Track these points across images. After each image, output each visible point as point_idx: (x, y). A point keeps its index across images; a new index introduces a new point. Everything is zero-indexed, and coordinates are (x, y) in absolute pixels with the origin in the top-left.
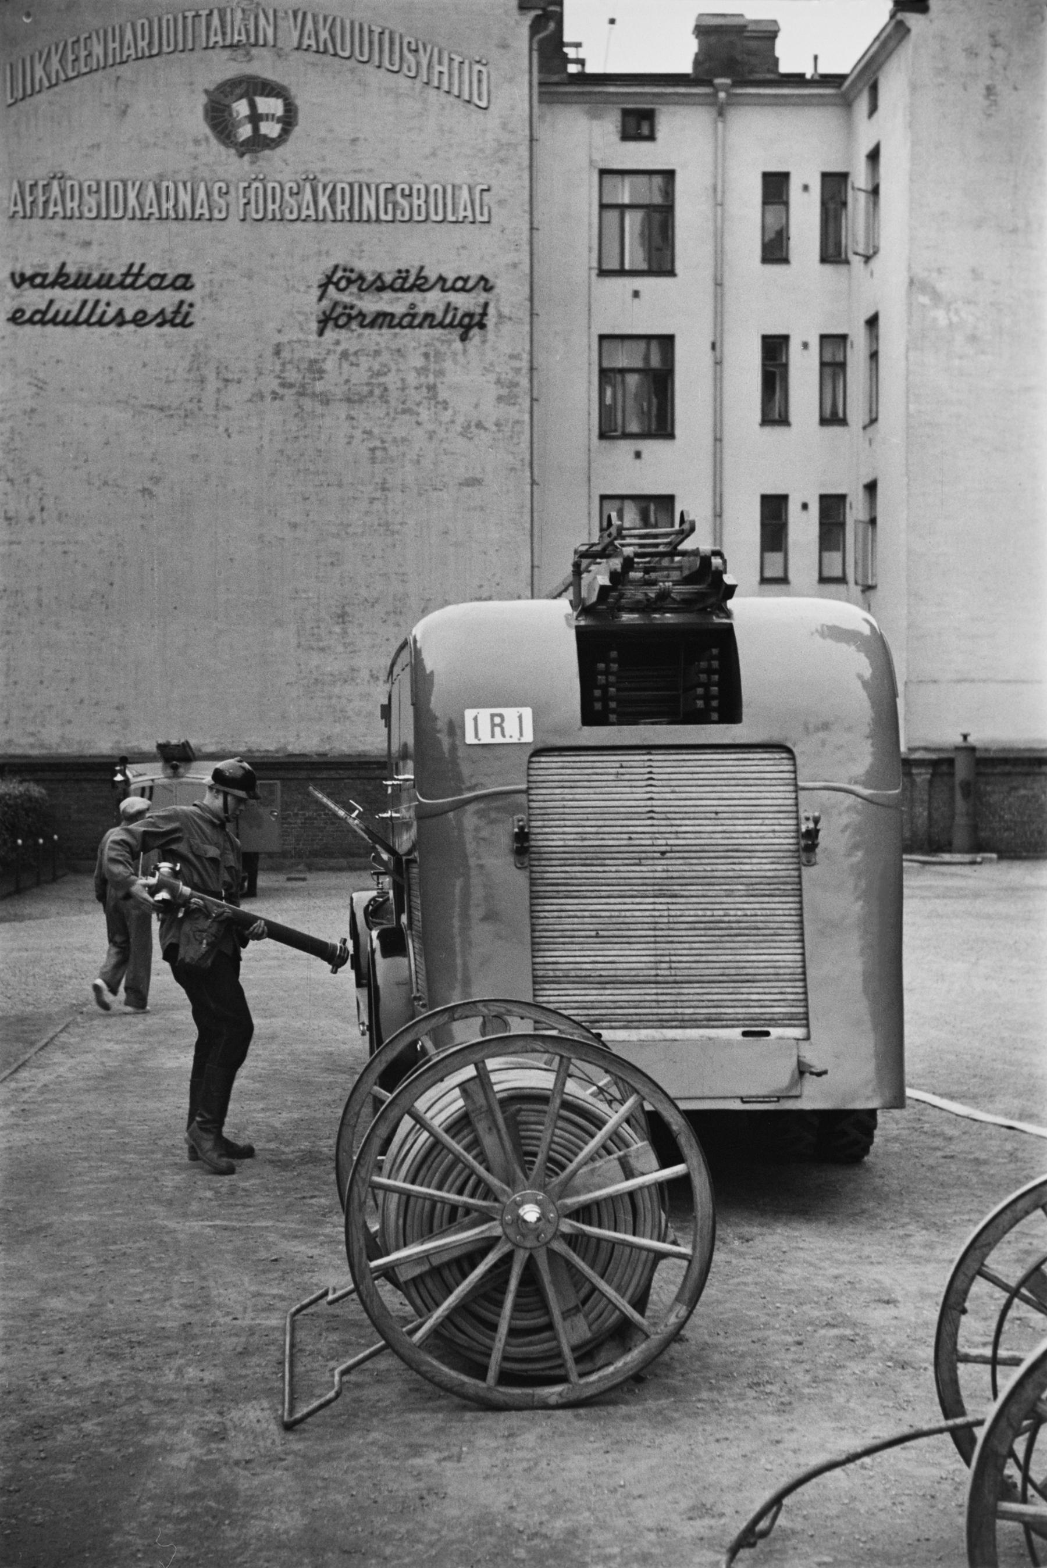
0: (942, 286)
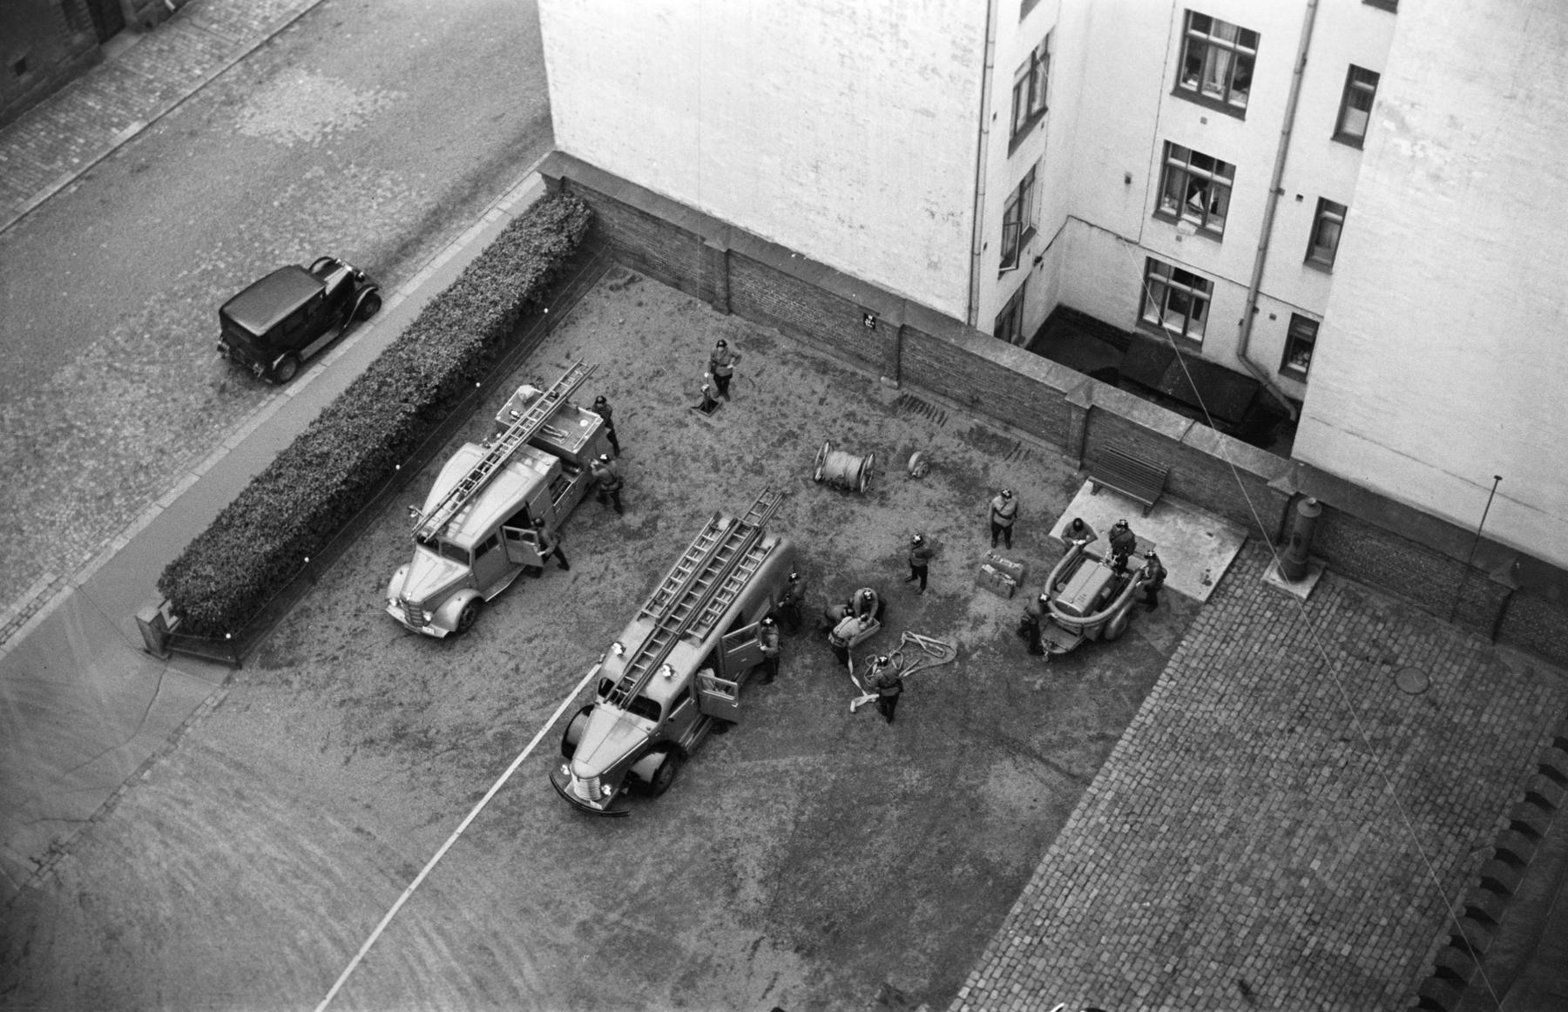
0: (1412, 119)
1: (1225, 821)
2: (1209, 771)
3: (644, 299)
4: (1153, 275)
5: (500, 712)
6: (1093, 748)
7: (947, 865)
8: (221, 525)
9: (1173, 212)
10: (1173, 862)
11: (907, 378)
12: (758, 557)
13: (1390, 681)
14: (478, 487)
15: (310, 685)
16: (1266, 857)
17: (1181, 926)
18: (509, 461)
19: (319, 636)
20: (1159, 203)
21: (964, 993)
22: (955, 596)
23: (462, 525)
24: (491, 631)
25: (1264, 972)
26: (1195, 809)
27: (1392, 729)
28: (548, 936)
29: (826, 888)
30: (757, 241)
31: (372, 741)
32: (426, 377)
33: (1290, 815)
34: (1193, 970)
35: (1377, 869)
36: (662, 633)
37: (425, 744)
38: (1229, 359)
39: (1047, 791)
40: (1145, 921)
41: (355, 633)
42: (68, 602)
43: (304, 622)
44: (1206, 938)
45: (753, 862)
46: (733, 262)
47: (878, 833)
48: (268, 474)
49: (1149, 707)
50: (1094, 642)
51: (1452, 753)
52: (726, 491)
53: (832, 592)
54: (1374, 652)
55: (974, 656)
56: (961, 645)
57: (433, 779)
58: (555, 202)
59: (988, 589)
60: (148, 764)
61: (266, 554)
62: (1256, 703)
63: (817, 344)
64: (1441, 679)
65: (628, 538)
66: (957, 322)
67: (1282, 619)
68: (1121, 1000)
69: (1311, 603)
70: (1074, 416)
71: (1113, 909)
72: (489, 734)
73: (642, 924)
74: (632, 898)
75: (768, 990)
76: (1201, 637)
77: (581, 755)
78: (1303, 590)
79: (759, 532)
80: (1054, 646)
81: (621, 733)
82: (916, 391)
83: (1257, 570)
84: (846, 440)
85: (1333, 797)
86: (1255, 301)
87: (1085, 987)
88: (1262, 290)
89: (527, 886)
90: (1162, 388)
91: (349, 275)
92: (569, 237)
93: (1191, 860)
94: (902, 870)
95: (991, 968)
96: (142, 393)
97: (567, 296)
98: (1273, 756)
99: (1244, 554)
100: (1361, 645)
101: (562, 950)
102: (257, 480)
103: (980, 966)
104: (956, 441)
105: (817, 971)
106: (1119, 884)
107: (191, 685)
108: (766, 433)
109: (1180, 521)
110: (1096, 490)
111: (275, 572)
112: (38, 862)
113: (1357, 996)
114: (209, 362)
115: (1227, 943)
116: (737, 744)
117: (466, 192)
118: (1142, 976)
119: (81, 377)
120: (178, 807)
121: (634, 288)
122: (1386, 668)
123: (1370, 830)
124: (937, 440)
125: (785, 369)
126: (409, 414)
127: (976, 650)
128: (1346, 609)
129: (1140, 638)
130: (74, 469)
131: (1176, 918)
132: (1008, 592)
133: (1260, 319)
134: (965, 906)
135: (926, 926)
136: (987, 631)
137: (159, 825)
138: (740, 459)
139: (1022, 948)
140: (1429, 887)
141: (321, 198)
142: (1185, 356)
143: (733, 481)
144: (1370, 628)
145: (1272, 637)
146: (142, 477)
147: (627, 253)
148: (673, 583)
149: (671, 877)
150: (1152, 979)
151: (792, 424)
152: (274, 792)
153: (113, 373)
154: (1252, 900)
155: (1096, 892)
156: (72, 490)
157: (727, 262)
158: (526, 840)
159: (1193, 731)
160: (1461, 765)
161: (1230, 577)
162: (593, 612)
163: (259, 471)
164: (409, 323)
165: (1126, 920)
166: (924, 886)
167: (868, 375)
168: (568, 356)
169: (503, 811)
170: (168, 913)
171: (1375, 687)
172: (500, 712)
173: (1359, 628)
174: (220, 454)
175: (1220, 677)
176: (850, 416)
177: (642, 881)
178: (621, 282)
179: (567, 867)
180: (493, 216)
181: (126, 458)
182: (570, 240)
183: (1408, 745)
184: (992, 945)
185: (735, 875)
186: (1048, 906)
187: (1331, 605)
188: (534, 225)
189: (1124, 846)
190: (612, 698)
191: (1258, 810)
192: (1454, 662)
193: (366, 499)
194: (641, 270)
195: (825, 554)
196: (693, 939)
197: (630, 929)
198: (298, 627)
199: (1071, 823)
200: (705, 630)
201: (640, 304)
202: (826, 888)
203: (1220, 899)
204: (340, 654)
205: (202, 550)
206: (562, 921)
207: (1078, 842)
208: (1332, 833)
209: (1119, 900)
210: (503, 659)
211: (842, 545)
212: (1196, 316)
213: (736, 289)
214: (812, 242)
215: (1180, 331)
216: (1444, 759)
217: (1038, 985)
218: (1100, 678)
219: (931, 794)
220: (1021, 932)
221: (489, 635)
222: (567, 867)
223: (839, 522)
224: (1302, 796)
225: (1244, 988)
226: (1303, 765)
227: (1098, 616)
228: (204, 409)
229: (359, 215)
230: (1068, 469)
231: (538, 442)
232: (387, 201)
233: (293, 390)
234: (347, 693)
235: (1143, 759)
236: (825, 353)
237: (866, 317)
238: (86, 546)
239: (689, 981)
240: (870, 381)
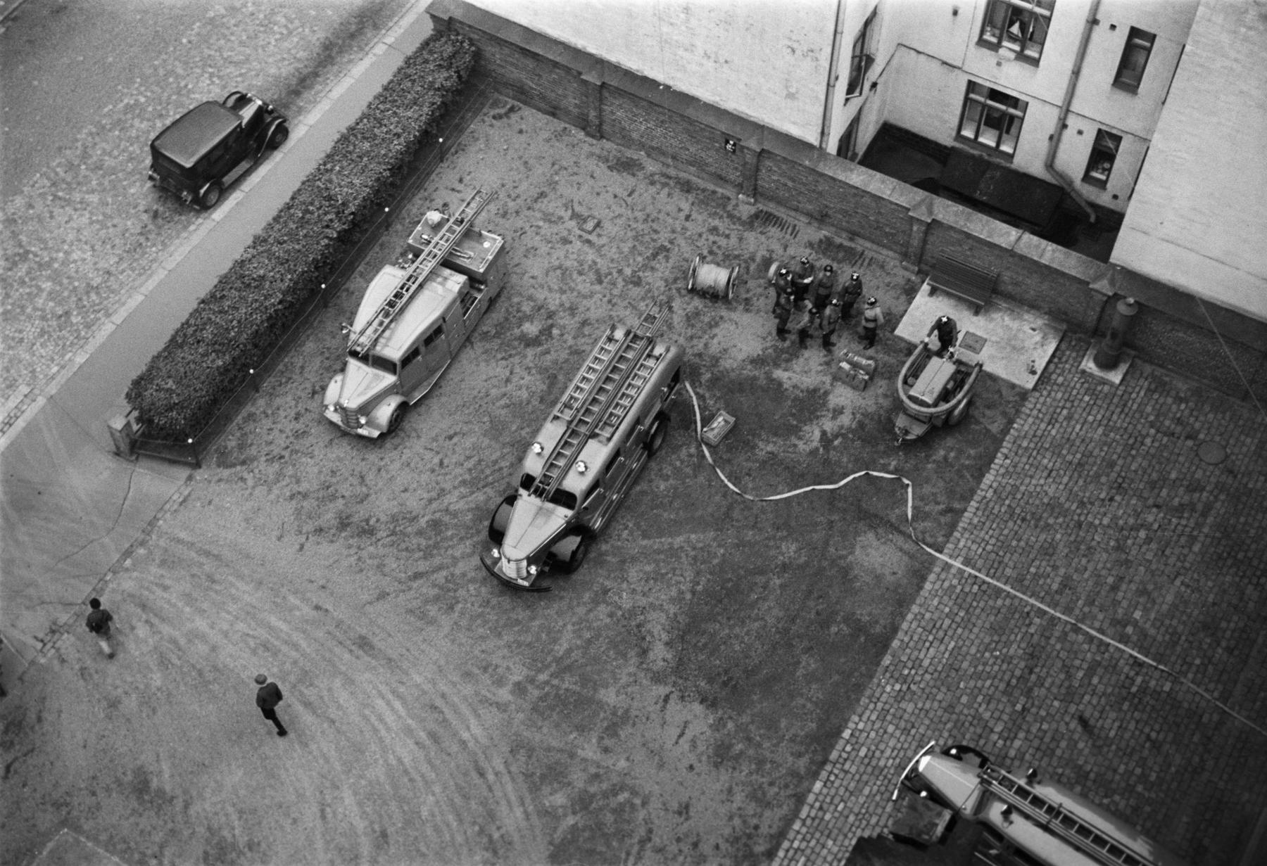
1: (1058, 580)
2: (1043, 537)
3: (524, 127)
4: (972, 96)
5: (430, 501)
6: (943, 520)
7: (825, 624)
8: (175, 343)
9: (994, 40)
10: (1017, 616)
11: (762, 195)
12: (651, 363)
13: (1192, 454)
14: (398, 303)
15: (262, 481)
16: (1095, 610)
17: (1027, 671)
18: (426, 280)
19: (266, 438)
20: (982, 32)
21: (846, 734)
22: (815, 390)
23: (389, 339)
24: (415, 430)
25: (1099, 708)
26: (1033, 570)
27: (1197, 495)
28: (488, 695)
29: (723, 647)
30: (628, 74)
31: (321, 530)
32: (343, 204)
33: (1114, 572)
34: (1040, 708)
35: (1190, 616)
36: (574, 433)
37: (367, 531)
38: (1036, 168)
39: (906, 558)
40: (996, 668)
41: (298, 435)
42: (43, 410)
43: (251, 426)
44: (1049, 680)
45: (659, 627)
46: (606, 94)
47: (765, 599)
48: (213, 296)
49: (988, 482)
50: (940, 428)
51: (1249, 514)
52: (610, 301)
53: (709, 388)
54: (1179, 429)
55: (836, 443)
56: (824, 433)
57: (376, 562)
58: (443, 40)
59: (844, 383)
60: (128, 553)
61: (218, 368)
62: (1080, 476)
63: (681, 166)
64: (1236, 450)
65: (527, 345)
66: (810, 146)
67: (1099, 402)
68: (980, 736)
69: (1122, 388)
70: (915, 228)
71: (969, 658)
72: (423, 522)
73: (568, 683)
74: (558, 660)
75: (680, 736)
76: (1030, 420)
77: (509, 541)
78: (1116, 377)
79: (651, 341)
80: (907, 432)
81: (540, 521)
82: (771, 207)
83: (1075, 359)
84: (711, 252)
85: (1149, 556)
86: (1065, 118)
87: (949, 726)
88: (1072, 109)
89: (467, 653)
90: (977, 195)
91: (260, 108)
92: (457, 72)
93: (1032, 614)
94: (787, 630)
95: (868, 713)
96: (85, 220)
97: (457, 125)
98: (1097, 522)
99: (1063, 346)
100: (1167, 423)
101: (502, 707)
102: (203, 302)
103: (859, 710)
104: (808, 251)
105: (721, 719)
106: (972, 637)
107: (156, 483)
108: (640, 248)
109: (1006, 318)
110: (933, 292)
111: (226, 383)
112: (42, 641)
113: (1178, 726)
114: (141, 191)
115: (1066, 684)
116: (637, 525)
117: (354, 27)
118: (997, 714)
119: (31, 206)
120: (159, 592)
121: (514, 117)
122: (1190, 443)
123: (1182, 583)
124: (791, 251)
125: (653, 190)
126: (331, 239)
127: (836, 437)
128: (1154, 391)
129: (978, 423)
130: (35, 290)
131: (1022, 664)
132: (862, 386)
133: (1069, 134)
134: (842, 660)
135: (811, 678)
136: (845, 420)
137: (144, 607)
138: (620, 272)
139: (894, 694)
140: (1234, 631)
141: (225, 36)
142: (998, 167)
143: (616, 292)
144: (1174, 407)
145: (1091, 418)
146: (93, 296)
147: (506, 85)
148: (580, 387)
149: (589, 642)
150: (1005, 717)
151: (663, 239)
152: (241, 577)
153: (58, 202)
154: (1086, 646)
155: (953, 644)
156: (35, 309)
157: (600, 93)
158: (462, 613)
159: (1027, 503)
160: (1256, 524)
161: (1052, 366)
162: (503, 412)
163: (203, 293)
164: (323, 155)
165: (980, 668)
166: (806, 643)
167: (728, 194)
168: (461, 181)
169: (441, 588)
170: (159, 683)
171: (1181, 459)
172: (430, 501)
173: (1164, 408)
174: (161, 275)
175: (1048, 455)
176: (714, 230)
177: (566, 646)
178: (502, 111)
179: (499, 635)
180: (380, 49)
181: (78, 280)
182: (459, 77)
183: (1210, 509)
184: (868, 692)
185: (644, 638)
186: (913, 657)
187: (1139, 394)
188: (426, 61)
189: (975, 604)
190: (535, 492)
191: (1086, 569)
192: (1247, 435)
193: (297, 315)
194: (519, 100)
195: (700, 355)
196: (613, 695)
197: (558, 688)
198: (247, 429)
199: (928, 586)
200: (611, 430)
201: (521, 132)
202: (723, 647)
203: (1058, 646)
204: (286, 454)
205: (161, 365)
206: (500, 682)
207: (935, 602)
208: (1150, 587)
209: (973, 650)
210: (428, 455)
211: (714, 348)
212: (1008, 132)
213: (608, 117)
214: (679, 75)
215: (993, 144)
216: (1242, 520)
217: (909, 726)
218: (945, 458)
219: (807, 564)
220: (892, 681)
221: (414, 434)
222: (499, 635)
223: (711, 327)
224: (1124, 556)
225: (1083, 721)
226: (1122, 529)
227: (944, 407)
228: (141, 234)
229: (260, 51)
230: (907, 274)
231: (448, 263)
232: (283, 38)
233: (218, 214)
234: (296, 488)
235: (986, 528)
236: (689, 174)
237: (727, 142)
238: (52, 360)
239: (612, 730)
240: (729, 199)
